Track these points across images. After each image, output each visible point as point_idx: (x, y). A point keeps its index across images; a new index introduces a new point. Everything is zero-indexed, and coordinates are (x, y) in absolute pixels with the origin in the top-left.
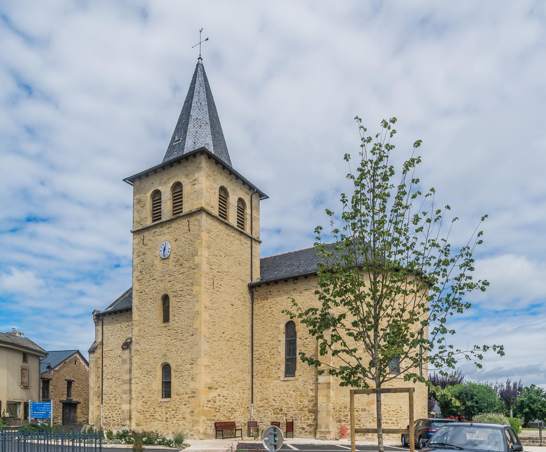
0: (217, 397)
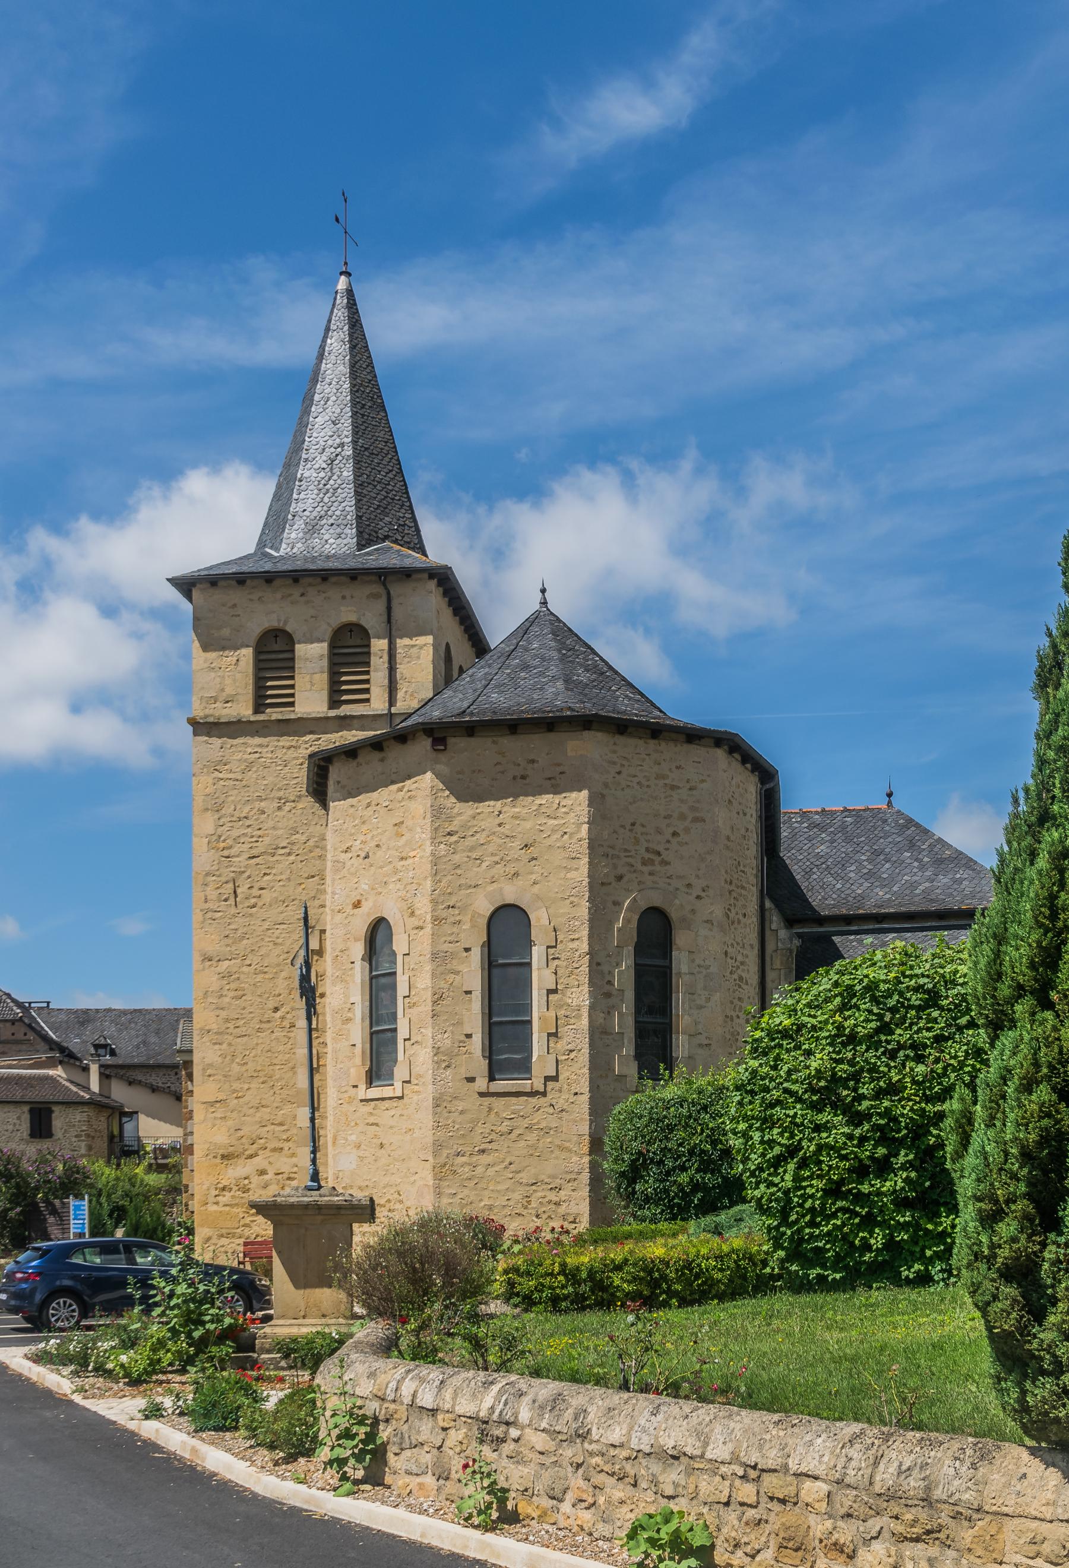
0: (255, 1180)
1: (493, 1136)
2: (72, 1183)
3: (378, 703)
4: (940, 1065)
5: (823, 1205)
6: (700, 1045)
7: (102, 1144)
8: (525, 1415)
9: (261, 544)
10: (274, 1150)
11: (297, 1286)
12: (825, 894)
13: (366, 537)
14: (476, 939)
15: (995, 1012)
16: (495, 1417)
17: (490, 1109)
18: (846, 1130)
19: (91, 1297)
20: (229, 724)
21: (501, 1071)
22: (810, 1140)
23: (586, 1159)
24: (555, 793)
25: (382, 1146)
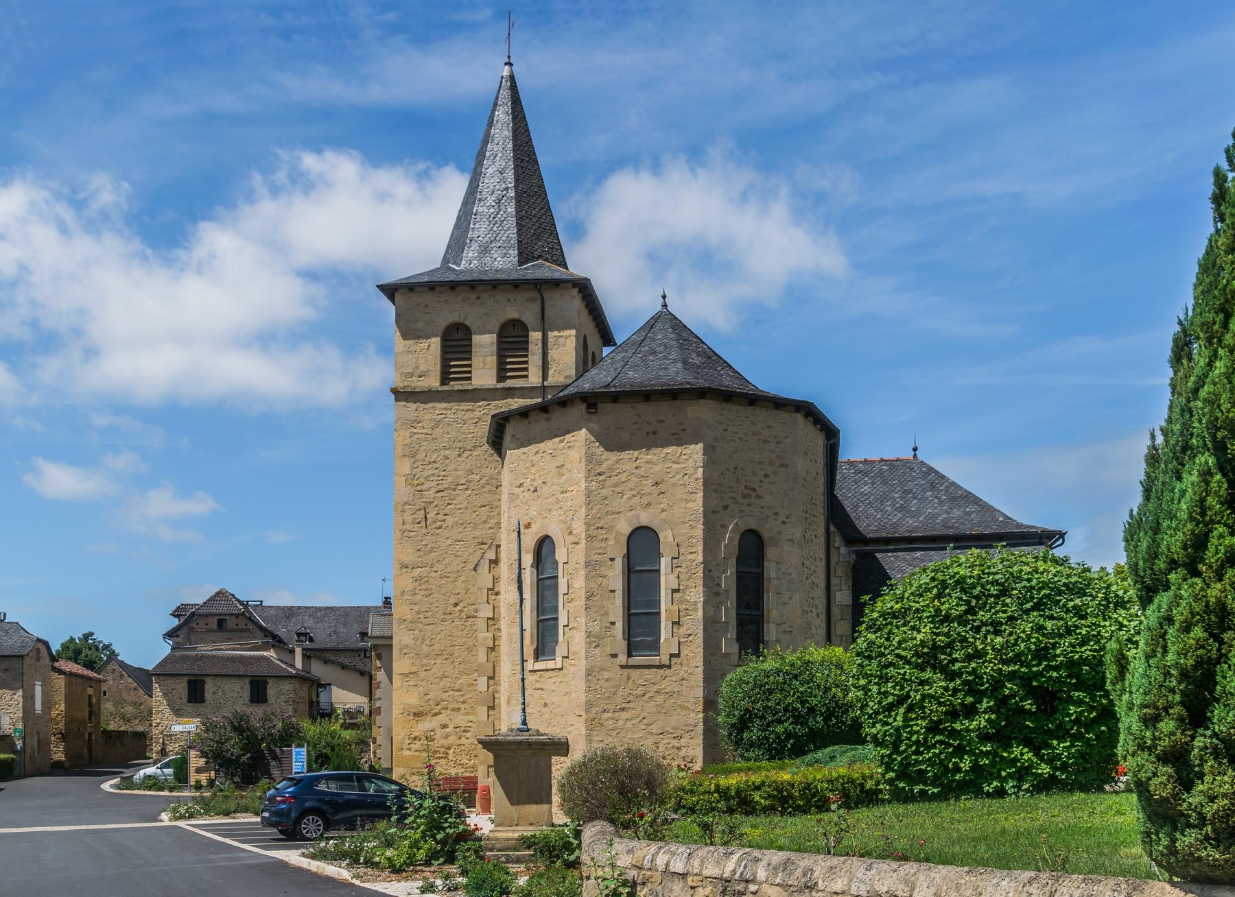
0: (439, 732)
1: (631, 698)
2: (290, 736)
3: (534, 378)
4: (1014, 637)
5: (925, 739)
6: (785, 632)
7: (304, 707)
8: (762, 874)
9: (446, 260)
10: (454, 710)
11: (512, 803)
12: (869, 522)
13: (525, 256)
14: (619, 552)
15: (1152, 579)
16: (737, 877)
17: (629, 678)
18: (943, 684)
19: (333, 814)
20: (422, 392)
21: (636, 650)
22: (916, 691)
23: (701, 716)
24: (679, 445)
25: (546, 705)
